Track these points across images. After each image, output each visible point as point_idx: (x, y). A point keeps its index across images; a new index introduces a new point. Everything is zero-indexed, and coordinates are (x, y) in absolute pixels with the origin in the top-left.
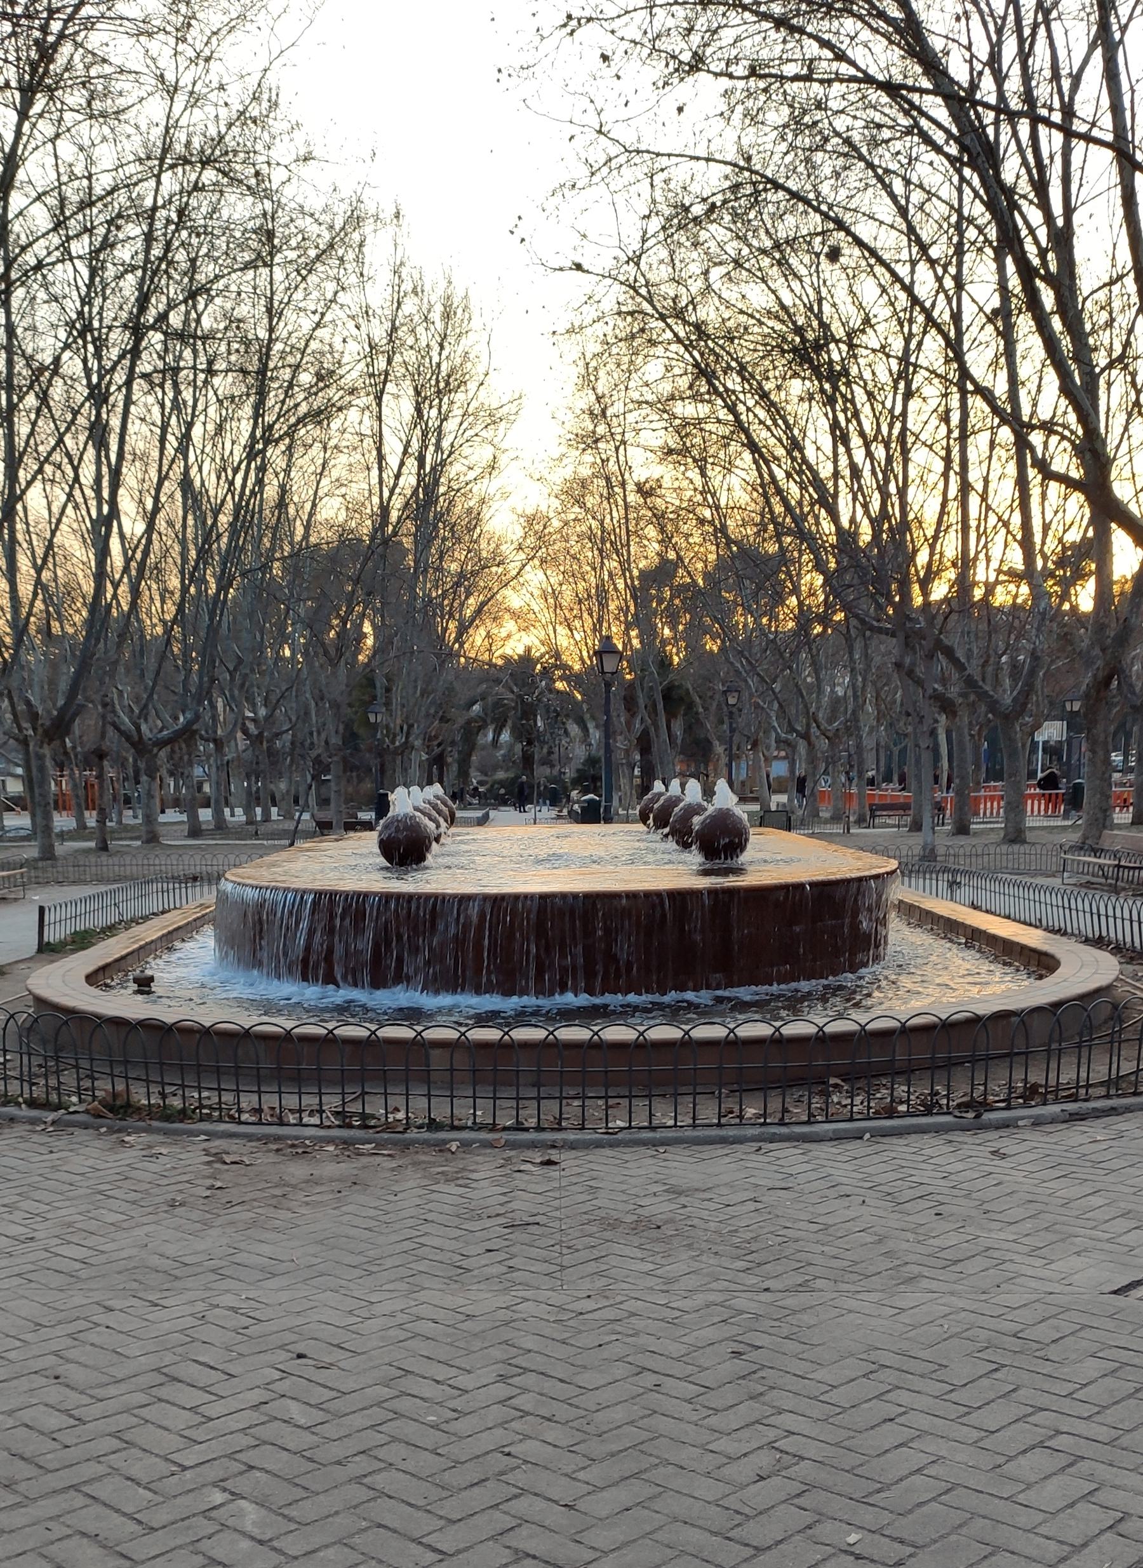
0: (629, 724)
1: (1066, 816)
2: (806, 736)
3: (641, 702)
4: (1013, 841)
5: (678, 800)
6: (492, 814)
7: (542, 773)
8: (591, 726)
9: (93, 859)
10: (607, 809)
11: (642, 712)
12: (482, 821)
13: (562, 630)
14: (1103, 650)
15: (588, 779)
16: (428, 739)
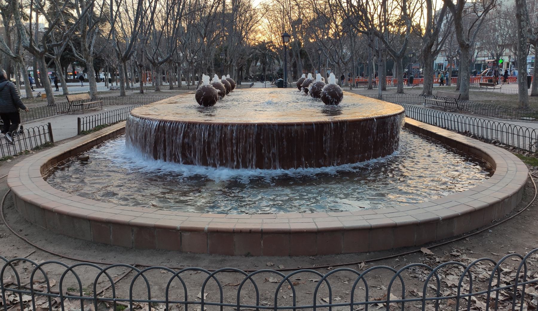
0: (291, 60)
1: (409, 85)
2: (338, 63)
3: (294, 54)
4: (400, 93)
5: (304, 79)
6: (255, 83)
7: (267, 73)
8: (281, 61)
9: (140, 97)
10: (286, 83)
11: (294, 57)
12: (251, 86)
13: (273, 35)
14: (430, 37)
15: (280, 74)
16: (238, 64)
